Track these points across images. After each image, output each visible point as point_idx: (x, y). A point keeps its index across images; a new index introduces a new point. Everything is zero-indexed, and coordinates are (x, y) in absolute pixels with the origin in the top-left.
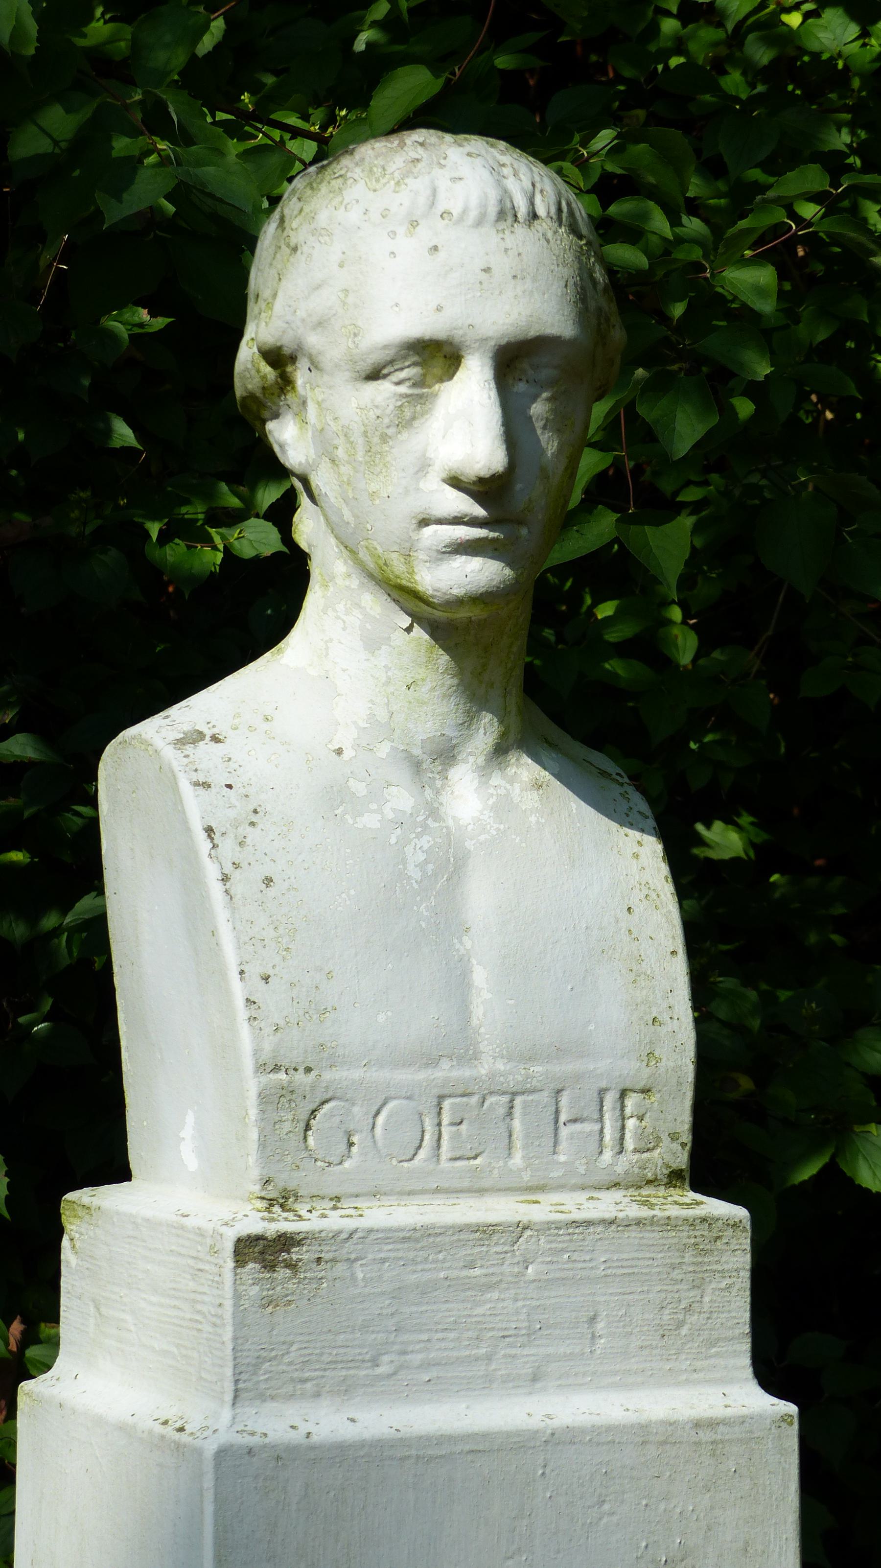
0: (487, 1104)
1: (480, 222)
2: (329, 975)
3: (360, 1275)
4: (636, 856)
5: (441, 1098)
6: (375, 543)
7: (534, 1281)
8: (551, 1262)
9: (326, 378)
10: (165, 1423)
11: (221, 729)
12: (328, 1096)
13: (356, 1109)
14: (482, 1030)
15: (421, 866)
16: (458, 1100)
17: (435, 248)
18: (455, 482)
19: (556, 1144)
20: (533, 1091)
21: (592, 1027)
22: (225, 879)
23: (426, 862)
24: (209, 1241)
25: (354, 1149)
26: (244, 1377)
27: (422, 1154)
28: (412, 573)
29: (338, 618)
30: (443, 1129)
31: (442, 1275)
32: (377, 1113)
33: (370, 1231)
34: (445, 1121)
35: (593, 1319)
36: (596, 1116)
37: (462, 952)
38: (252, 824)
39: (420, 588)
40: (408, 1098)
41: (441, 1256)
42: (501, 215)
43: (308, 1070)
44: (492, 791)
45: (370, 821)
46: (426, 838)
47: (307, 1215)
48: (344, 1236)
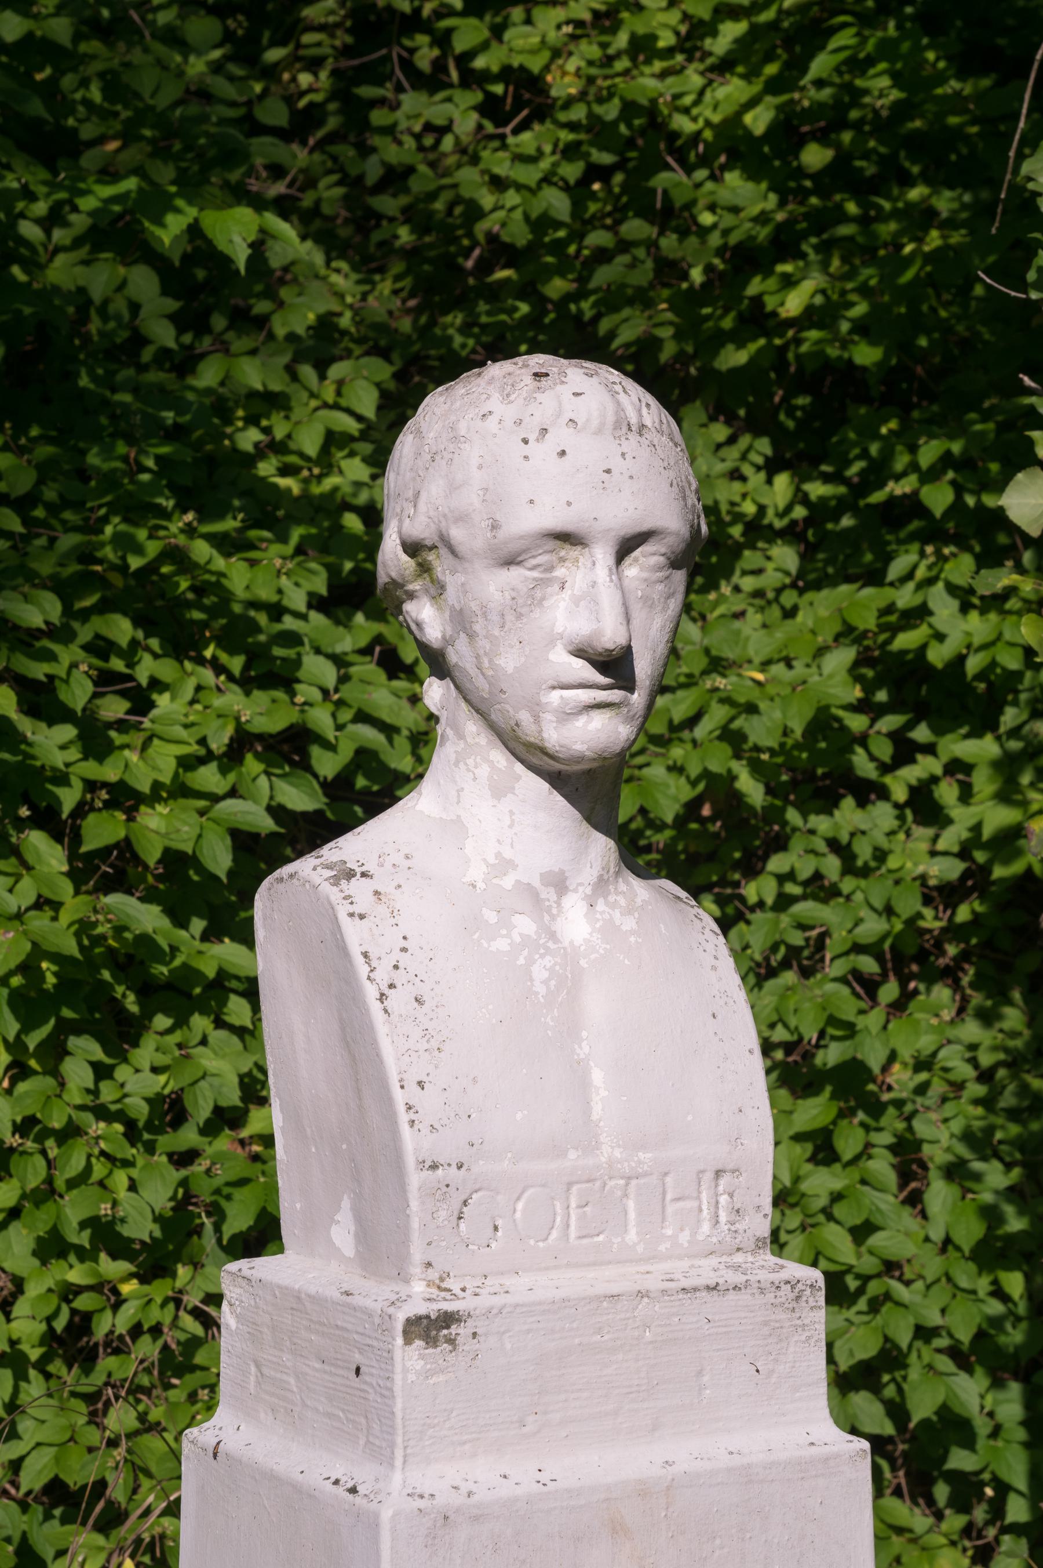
0: (607, 1188)
1: (599, 431)
2: (475, 1080)
3: (508, 1346)
4: (714, 968)
5: (570, 1185)
6: (507, 707)
7: (651, 1342)
8: (666, 1325)
9: (467, 565)
10: (336, 1482)
11: (370, 867)
12: (477, 1187)
13: (500, 1198)
14: (602, 1124)
15: (546, 982)
16: (584, 1186)
17: (563, 453)
18: (580, 653)
19: (663, 1220)
20: (646, 1174)
21: (690, 1118)
22: (382, 997)
23: (549, 979)
24: (377, 1320)
25: (499, 1234)
26: (411, 1443)
27: (554, 1234)
28: (540, 731)
29: (469, 770)
30: (572, 1212)
31: (577, 1341)
32: (518, 1199)
33: (517, 1306)
34: (573, 1205)
35: (700, 1373)
36: (695, 1195)
37: (582, 1056)
38: (404, 950)
39: (547, 745)
40: (543, 1186)
41: (575, 1325)
42: (617, 425)
43: (460, 1167)
44: (598, 916)
45: (501, 944)
46: (548, 958)
47: (461, 1294)
48: (494, 1311)
